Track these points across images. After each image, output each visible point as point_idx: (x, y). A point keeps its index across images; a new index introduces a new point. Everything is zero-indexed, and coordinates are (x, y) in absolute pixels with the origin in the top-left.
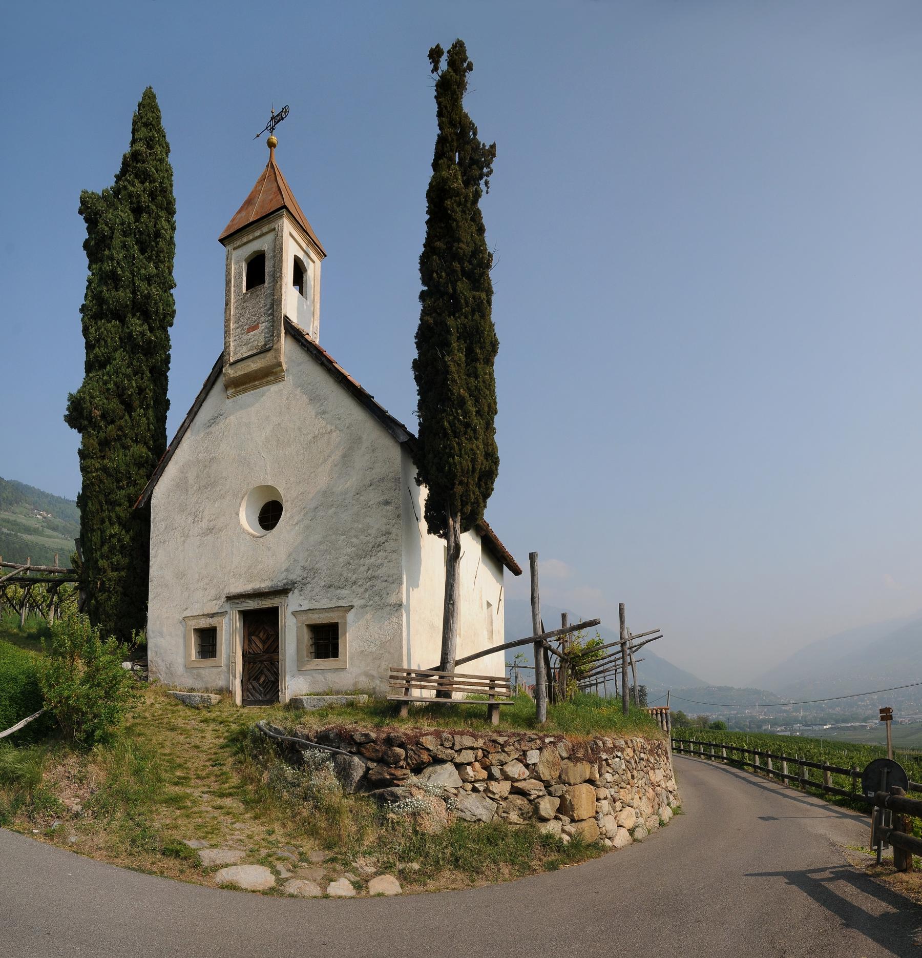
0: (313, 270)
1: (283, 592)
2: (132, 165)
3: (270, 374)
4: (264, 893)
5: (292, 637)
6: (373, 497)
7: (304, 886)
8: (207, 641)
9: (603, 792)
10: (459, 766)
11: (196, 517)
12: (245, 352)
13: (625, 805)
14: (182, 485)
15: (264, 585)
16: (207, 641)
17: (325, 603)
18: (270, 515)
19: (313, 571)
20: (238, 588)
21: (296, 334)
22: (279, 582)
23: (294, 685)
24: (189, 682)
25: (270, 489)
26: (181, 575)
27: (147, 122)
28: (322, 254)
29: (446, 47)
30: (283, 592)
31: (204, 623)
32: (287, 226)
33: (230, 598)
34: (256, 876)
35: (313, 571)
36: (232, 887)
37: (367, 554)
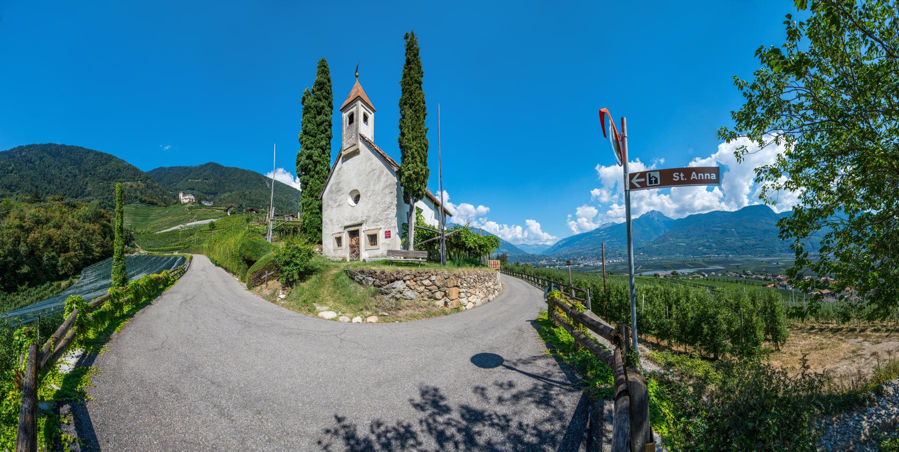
0: (371, 117)
1: (360, 225)
2: (320, 85)
3: (356, 152)
4: (332, 319)
5: (363, 238)
6: (387, 191)
7: (345, 319)
8: (339, 240)
9: (461, 290)
10: (405, 281)
11: (335, 202)
12: (348, 146)
13: (471, 294)
14: (331, 192)
15: (356, 222)
16: (339, 240)
17: (373, 227)
18: (357, 199)
19: (369, 217)
20: (348, 224)
21: (363, 138)
22: (359, 221)
23: (365, 255)
24: (333, 254)
25: (356, 191)
26: (331, 220)
27: (323, 69)
28: (374, 111)
29: (410, 33)
30: (360, 225)
31: (338, 236)
32: (359, 103)
33: (346, 227)
34: (331, 315)
35: (369, 217)
36: (322, 318)
37: (385, 210)
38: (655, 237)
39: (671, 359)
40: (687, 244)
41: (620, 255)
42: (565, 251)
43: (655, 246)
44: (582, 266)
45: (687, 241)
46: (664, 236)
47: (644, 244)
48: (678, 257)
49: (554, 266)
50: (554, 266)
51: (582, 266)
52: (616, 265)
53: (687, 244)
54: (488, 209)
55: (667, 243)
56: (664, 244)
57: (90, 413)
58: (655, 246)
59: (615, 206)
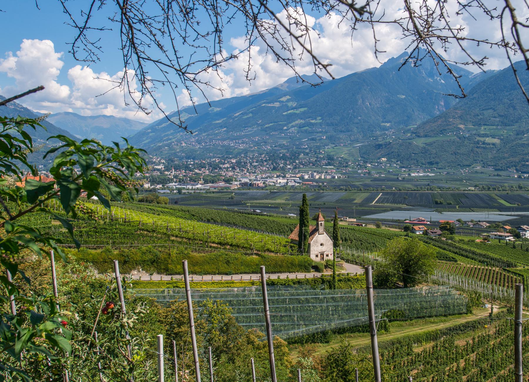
38: (419, 119)
39: (159, 34)
40: (505, 141)
41: (330, 160)
42: (186, 143)
43: (420, 142)
44: (235, 185)
45: (504, 132)
46: (444, 116)
47: (391, 136)
48: (477, 175)
49: (164, 181)
50: (164, 181)
51: (235, 185)
52: (320, 186)
53: (505, 141)
54: (62, 53)
55: (451, 136)
56: (441, 138)
57: (228, 95)
58: (420, 142)
59: (45, 261)
